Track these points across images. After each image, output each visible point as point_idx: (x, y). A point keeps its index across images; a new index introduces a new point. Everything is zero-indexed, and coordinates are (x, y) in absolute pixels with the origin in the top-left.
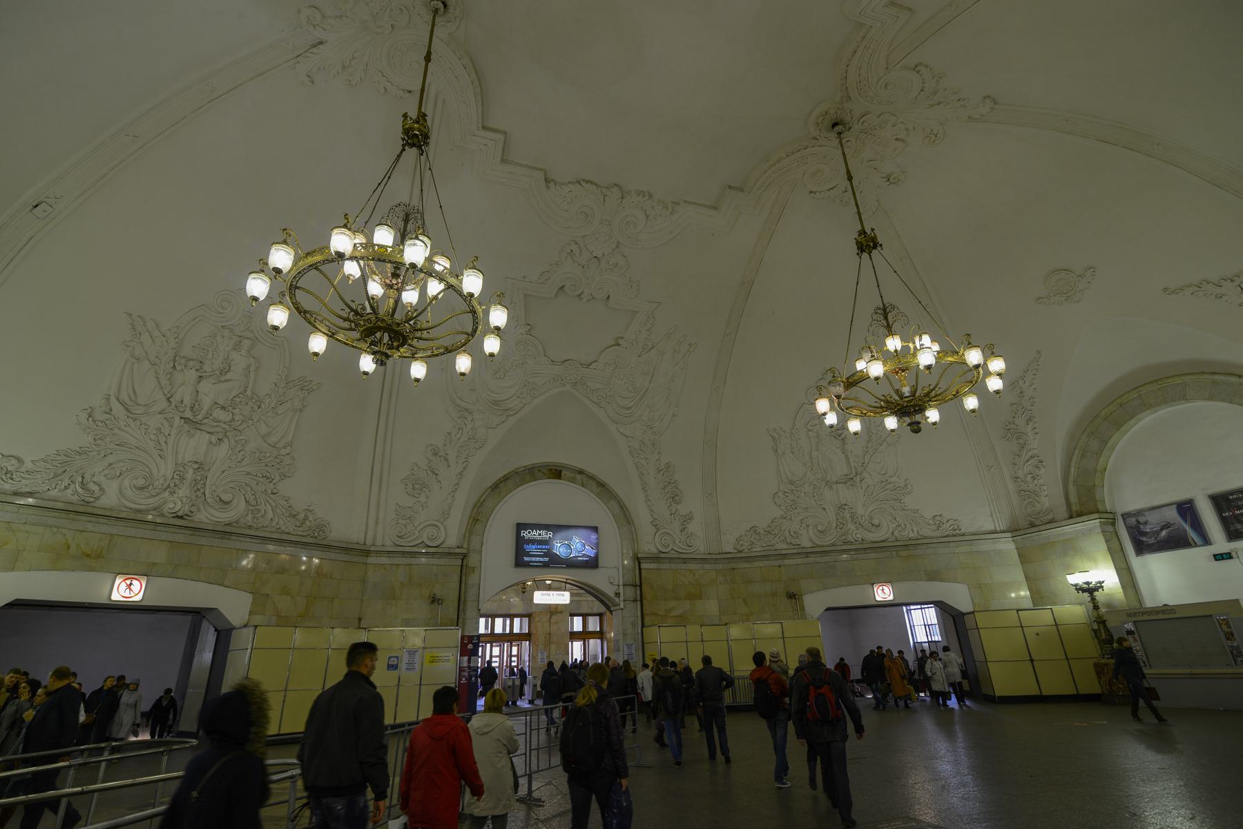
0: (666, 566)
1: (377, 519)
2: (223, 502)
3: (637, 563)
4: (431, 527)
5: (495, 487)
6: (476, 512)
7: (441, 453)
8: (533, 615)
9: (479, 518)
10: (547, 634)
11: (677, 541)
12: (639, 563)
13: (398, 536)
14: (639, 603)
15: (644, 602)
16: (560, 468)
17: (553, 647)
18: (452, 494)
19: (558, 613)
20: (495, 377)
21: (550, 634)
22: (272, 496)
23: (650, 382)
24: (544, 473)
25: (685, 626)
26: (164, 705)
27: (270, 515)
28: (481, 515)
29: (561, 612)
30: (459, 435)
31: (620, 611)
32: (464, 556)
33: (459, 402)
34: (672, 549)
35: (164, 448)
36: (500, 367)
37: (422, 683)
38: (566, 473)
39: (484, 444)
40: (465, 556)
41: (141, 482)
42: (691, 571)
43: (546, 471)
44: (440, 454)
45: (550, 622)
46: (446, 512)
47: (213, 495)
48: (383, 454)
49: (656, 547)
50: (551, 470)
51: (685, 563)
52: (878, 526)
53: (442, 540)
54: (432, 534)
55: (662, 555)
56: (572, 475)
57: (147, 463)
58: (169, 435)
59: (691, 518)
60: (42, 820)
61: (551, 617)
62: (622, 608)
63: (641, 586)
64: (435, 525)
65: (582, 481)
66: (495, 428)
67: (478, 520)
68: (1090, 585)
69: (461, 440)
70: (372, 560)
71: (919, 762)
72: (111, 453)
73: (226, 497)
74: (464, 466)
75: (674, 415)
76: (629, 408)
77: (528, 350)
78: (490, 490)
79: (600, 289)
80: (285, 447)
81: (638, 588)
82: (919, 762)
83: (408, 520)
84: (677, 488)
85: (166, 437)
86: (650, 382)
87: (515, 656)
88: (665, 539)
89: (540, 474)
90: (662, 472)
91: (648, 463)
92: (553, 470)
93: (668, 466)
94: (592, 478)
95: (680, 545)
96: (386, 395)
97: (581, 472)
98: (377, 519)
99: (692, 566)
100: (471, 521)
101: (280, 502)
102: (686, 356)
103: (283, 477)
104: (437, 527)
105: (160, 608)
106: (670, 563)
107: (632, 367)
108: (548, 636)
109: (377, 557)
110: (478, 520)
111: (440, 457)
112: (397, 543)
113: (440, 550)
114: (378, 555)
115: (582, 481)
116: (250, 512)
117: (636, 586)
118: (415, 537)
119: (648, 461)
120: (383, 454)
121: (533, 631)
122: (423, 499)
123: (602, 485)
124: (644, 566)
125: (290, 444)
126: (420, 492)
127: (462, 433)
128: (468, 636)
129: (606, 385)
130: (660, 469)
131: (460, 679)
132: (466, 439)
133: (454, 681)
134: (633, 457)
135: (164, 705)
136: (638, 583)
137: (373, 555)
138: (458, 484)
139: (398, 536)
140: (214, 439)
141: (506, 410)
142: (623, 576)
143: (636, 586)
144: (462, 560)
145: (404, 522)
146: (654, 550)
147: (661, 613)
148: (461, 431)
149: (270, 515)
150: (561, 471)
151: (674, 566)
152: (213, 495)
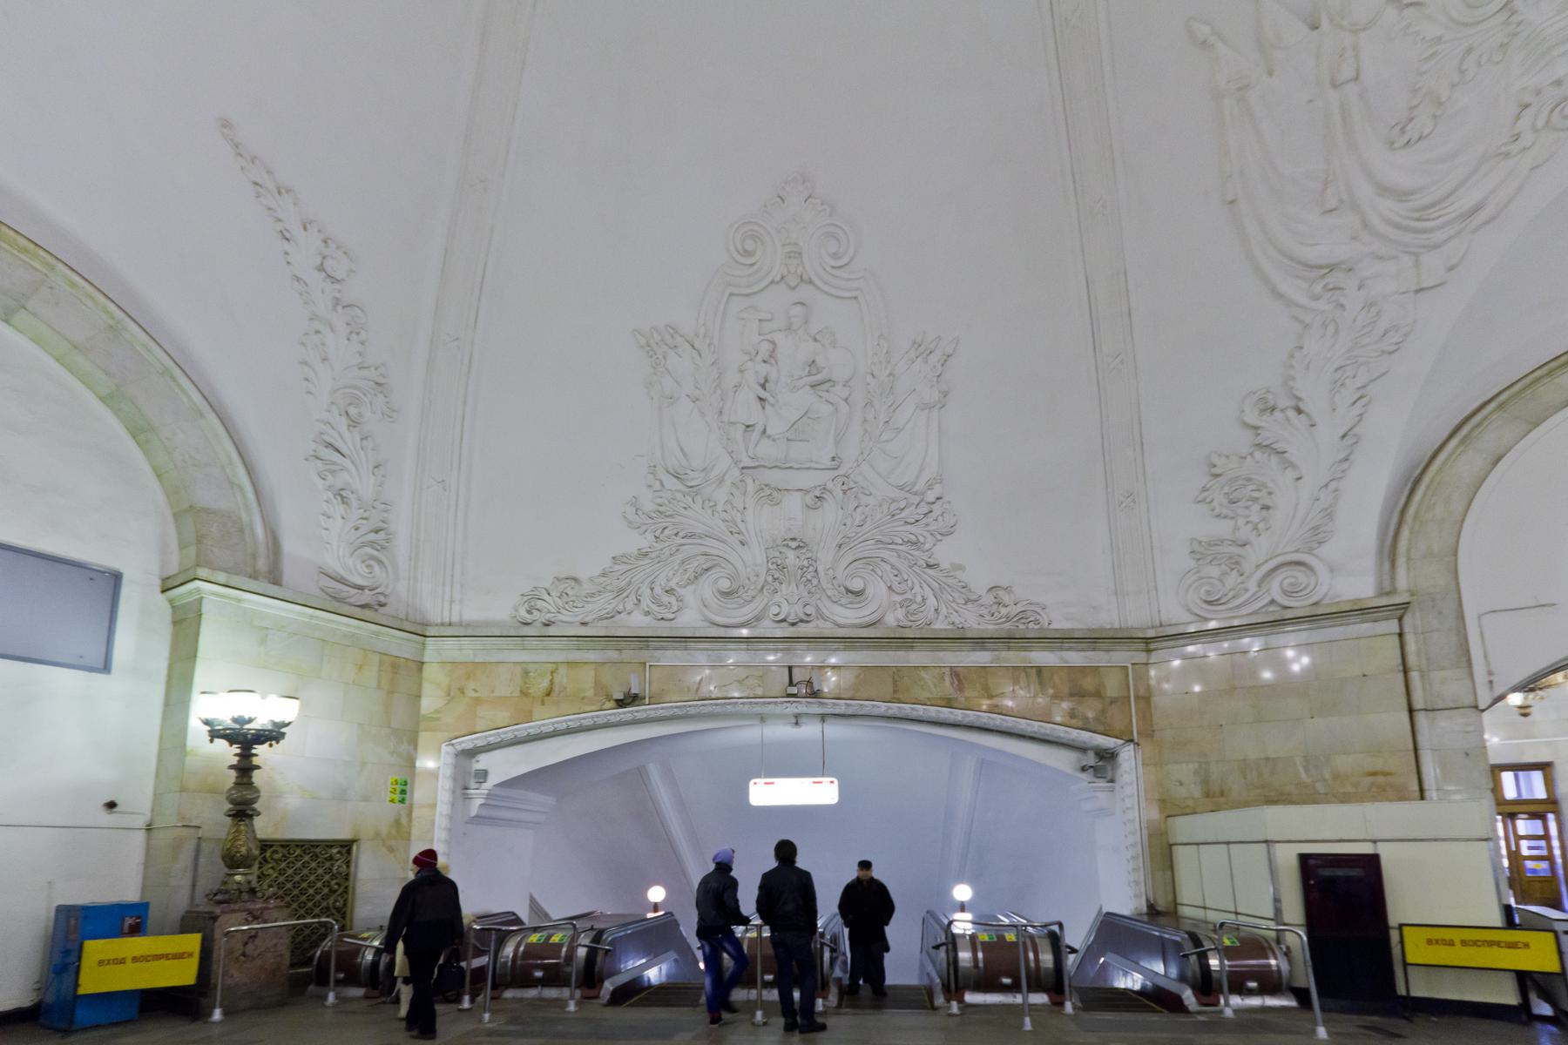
2: (852, 592)
4: (1285, 569)
13: (1209, 603)
22: (928, 571)
26: (1239, 945)
27: (932, 602)
35: (744, 530)
41: (725, 584)
47: (833, 585)
52: (858, 594)
57: (720, 554)
58: (745, 508)
60: (621, 983)
68: (247, 726)
72: (677, 550)
73: (857, 585)
74: (1358, 409)
80: (930, 488)
85: (742, 513)
101: (945, 581)
103: (939, 537)
105: (13, 547)
111: (1282, 411)
116: (898, 606)
118: (1247, 595)
125: (939, 480)
135: (1239, 945)
138: (1346, 459)
140: (809, 499)
148: (1331, 329)
149: (932, 602)
152: (833, 585)
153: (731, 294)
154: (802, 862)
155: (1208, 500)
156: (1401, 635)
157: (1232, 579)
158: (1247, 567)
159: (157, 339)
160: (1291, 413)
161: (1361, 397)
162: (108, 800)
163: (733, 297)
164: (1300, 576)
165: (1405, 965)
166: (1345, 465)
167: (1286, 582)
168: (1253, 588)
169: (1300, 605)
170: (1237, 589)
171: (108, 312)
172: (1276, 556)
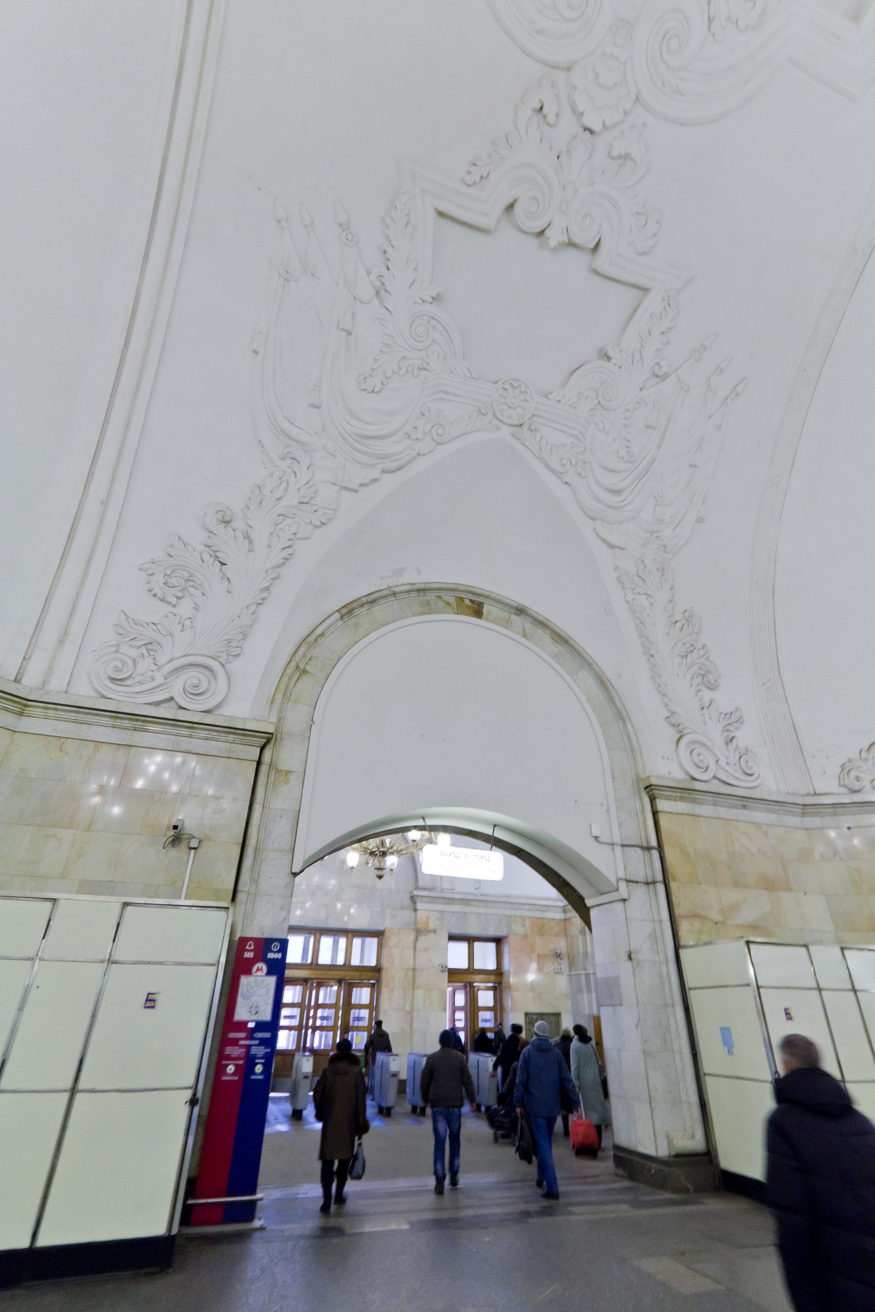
0: (706, 810)
1: (65, 633)
3: (647, 801)
5: (348, 611)
6: (304, 655)
7: (238, 524)
8: (386, 934)
9: (308, 668)
10: (408, 970)
11: (723, 762)
12: (652, 800)
13: (113, 680)
14: (661, 888)
15: (673, 886)
16: (480, 599)
17: (419, 993)
18: (253, 608)
19: (429, 931)
20: (364, 387)
21: (414, 969)
23: (659, 446)
24: (449, 604)
25: (806, 946)
28: (313, 662)
29: (435, 931)
30: (279, 493)
31: (620, 905)
32: (267, 740)
33: (285, 425)
34: (715, 777)
36: (374, 367)
37: (81, 1085)
38: (491, 608)
39: (330, 520)
40: (268, 741)
42: (758, 825)
43: (452, 600)
44: (234, 525)
45: (415, 948)
46: (235, 644)
48: (105, 503)
49: (682, 767)
50: (462, 599)
51: (744, 807)
53: (219, 698)
54: (196, 681)
55: (698, 786)
56: (505, 615)
59: (740, 721)
61: (416, 939)
62: (625, 896)
63: (660, 847)
64: (205, 667)
65: (524, 629)
66: (356, 491)
67: (305, 672)
69: (283, 503)
70: (34, 723)
71: (255, 988)
74: (285, 554)
75: (700, 520)
76: (617, 492)
77: (433, 341)
78: (337, 615)
79: (585, 216)
81: (655, 854)
82: (255, 988)
83: (143, 650)
84: (707, 659)
86: (659, 446)
87: (460, 1009)
88: (698, 755)
89: (440, 603)
90: (679, 625)
91: (652, 604)
92: (467, 602)
93: (689, 617)
94: (543, 624)
95: (728, 768)
96: (127, 381)
97: (520, 611)
98: (65, 633)
99: (760, 816)
100: (289, 671)
102: (729, 400)
104: (210, 670)
106: (714, 804)
107: (627, 410)
108: (410, 973)
109: (46, 718)
110: (305, 672)
112: (105, 693)
113: (209, 719)
114: (51, 713)
115: (524, 629)
117: (649, 849)
118: (154, 684)
119: (651, 600)
120: (105, 503)
121: (385, 963)
122: (185, 609)
123: (560, 638)
124: (661, 805)
126: (180, 594)
127: (286, 490)
128: (256, 940)
129: (577, 438)
130: (675, 619)
131: (220, 1069)
132: (295, 502)
133: (191, 1082)
134: (624, 589)
136: (654, 843)
137: (38, 711)
138: (267, 589)
139: (113, 680)
141: (383, 457)
142: (620, 824)
143: (649, 849)
144: (262, 749)
145: (133, 653)
146: (679, 775)
147: (715, 915)
148: (284, 485)
150: (480, 605)
151: (723, 812)
153: (126, 904)
154: (384, 1027)
155: (150, 572)
156: (259, 763)
157: (145, 665)
158: (162, 659)
159: (91, 963)
160: (240, 536)
161: (289, 547)
162: (790, 1022)
163: (129, 908)
164: (202, 677)
165: (539, 628)
166: (265, 595)
167: (188, 682)
168: (159, 680)
169: (194, 710)
170: (146, 676)
171: (484, 1189)
172: (190, 655)
